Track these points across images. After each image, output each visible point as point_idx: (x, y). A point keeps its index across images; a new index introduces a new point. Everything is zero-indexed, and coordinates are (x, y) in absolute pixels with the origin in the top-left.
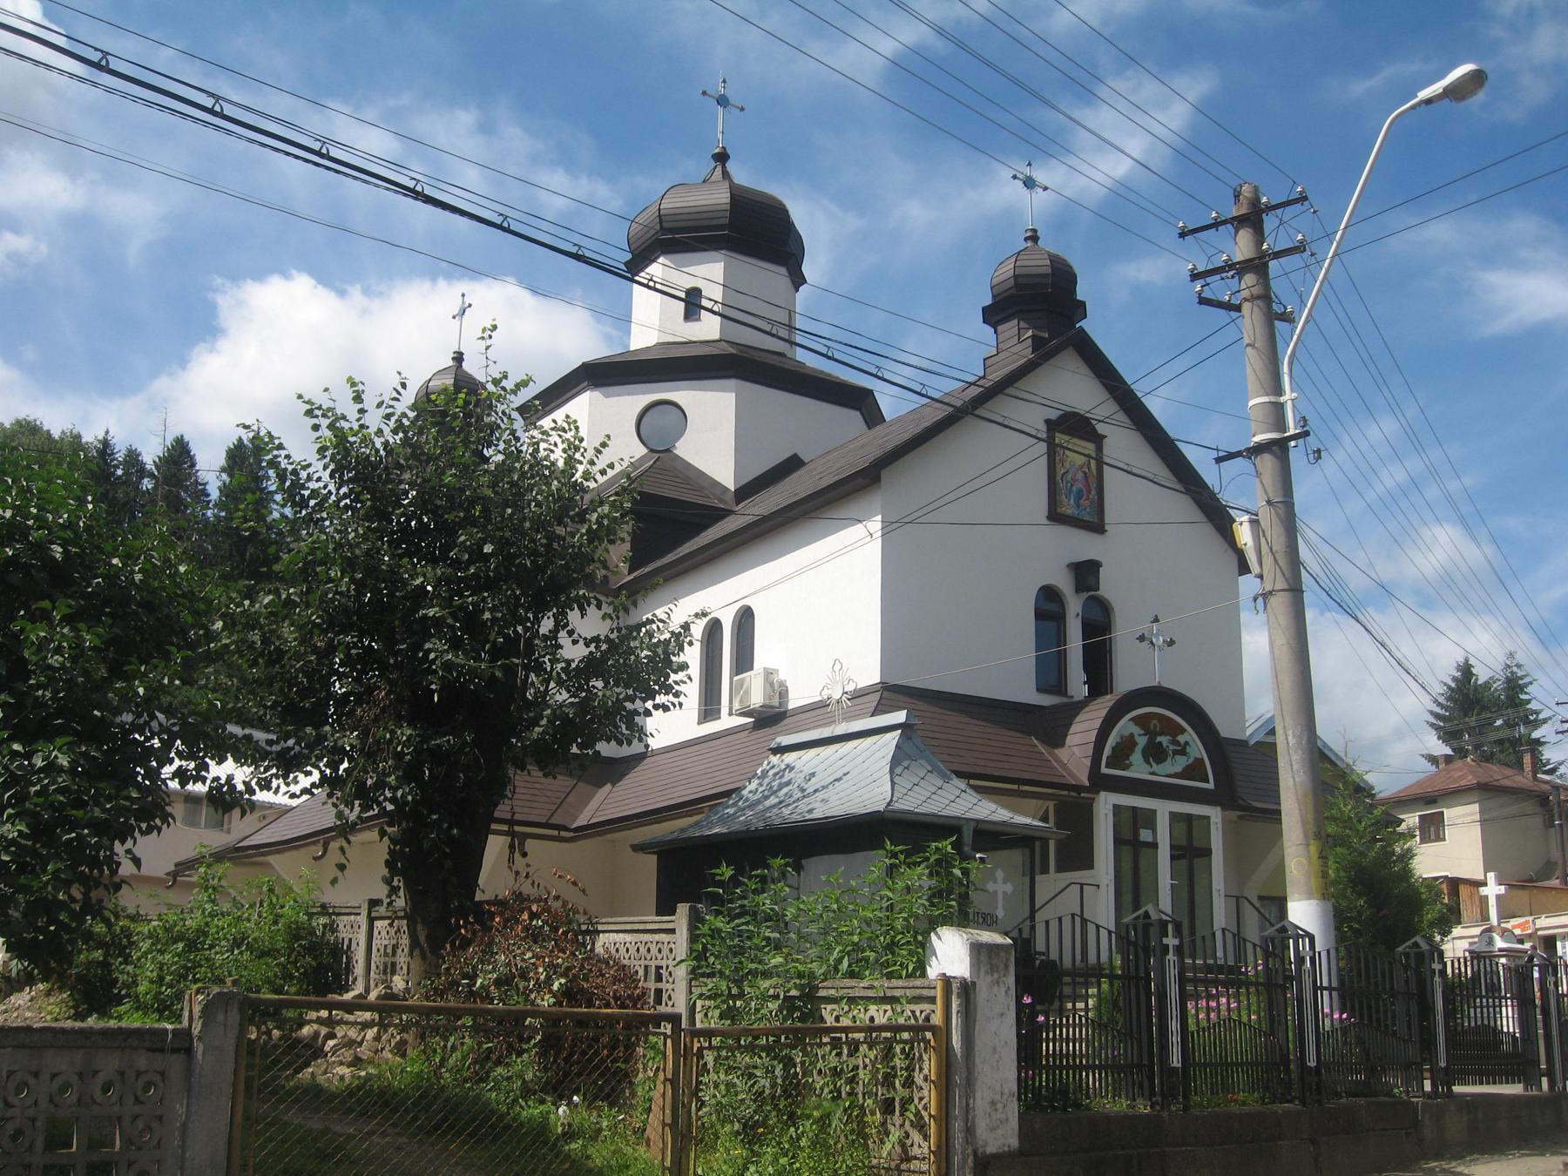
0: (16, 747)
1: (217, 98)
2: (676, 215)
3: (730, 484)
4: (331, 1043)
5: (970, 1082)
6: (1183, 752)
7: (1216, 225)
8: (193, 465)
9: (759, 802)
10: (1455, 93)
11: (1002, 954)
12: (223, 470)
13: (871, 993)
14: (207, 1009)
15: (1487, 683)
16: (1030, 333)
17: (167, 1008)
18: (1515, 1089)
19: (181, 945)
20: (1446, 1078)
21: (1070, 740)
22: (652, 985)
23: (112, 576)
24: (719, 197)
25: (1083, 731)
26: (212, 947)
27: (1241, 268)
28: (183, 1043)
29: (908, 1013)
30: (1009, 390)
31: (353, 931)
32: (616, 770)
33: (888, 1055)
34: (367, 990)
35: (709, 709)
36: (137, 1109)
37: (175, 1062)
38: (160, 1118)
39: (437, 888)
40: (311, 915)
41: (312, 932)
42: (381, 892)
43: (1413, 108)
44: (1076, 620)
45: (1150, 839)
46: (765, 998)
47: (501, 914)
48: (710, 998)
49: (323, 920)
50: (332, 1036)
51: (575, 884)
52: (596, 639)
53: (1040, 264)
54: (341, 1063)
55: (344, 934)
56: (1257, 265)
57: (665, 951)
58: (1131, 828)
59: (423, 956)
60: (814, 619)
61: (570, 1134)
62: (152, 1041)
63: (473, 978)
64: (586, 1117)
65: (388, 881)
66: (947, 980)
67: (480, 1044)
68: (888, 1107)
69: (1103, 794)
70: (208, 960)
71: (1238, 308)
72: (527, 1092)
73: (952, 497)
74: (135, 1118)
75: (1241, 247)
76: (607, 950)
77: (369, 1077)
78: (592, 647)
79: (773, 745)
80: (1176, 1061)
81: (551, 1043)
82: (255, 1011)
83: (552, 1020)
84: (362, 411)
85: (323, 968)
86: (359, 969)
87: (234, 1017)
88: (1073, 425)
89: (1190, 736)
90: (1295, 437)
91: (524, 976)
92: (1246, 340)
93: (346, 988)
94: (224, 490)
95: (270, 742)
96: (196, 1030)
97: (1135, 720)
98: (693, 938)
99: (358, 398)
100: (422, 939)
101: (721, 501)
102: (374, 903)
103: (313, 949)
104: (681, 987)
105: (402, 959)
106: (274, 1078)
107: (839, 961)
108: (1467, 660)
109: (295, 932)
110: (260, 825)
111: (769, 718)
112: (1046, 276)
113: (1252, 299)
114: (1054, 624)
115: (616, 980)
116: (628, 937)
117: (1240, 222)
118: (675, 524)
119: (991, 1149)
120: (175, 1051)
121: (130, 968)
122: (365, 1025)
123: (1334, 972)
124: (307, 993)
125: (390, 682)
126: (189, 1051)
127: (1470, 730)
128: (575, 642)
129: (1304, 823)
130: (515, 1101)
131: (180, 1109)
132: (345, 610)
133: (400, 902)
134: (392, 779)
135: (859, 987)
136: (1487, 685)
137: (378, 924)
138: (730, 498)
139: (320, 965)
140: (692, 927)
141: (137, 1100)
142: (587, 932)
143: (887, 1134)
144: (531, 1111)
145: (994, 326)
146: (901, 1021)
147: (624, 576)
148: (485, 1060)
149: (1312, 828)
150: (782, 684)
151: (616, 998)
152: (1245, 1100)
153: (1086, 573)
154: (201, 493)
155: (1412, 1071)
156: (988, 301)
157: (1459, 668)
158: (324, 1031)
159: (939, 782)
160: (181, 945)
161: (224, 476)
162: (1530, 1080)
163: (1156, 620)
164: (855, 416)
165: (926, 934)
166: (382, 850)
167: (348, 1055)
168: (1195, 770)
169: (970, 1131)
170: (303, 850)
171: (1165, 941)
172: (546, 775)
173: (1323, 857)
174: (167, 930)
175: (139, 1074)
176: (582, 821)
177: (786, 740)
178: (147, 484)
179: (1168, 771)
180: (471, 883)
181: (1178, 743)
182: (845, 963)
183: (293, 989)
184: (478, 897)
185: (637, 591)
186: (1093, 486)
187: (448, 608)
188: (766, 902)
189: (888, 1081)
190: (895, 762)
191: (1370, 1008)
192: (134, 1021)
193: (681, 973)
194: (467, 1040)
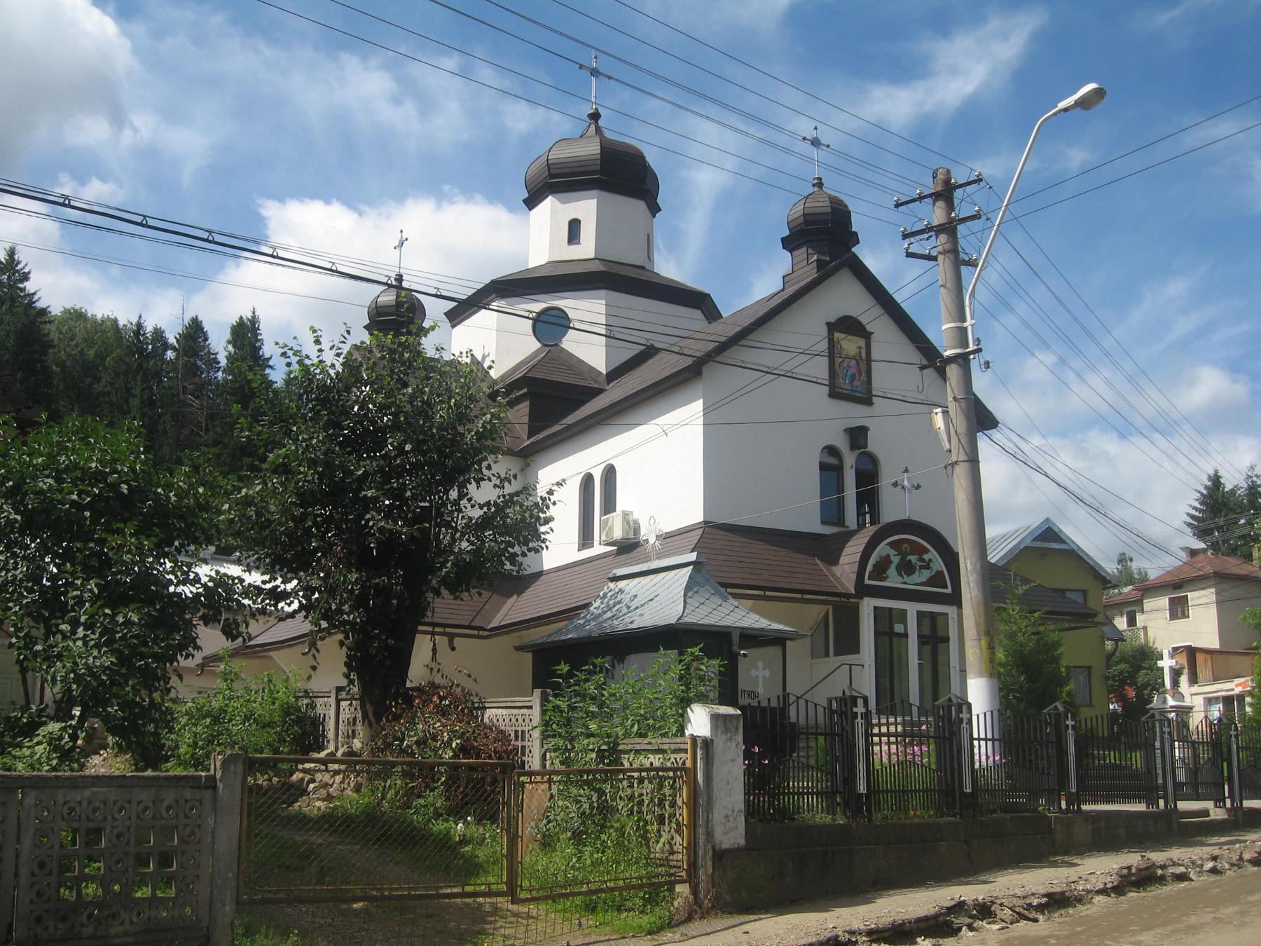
0: (107, 611)
1: (210, 232)
2: (561, 164)
3: (603, 369)
4: (312, 786)
5: (709, 805)
6: (928, 567)
7: (921, 198)
8: (206, 339)
9: (600, 615)
10: (1083, 103)
11: (734, 721)
12: (229, 342)
13: (649, 747)
14: (225, 764)
15: (1232, 490)
16: (815, 258)
17: (201, 764)
18: (1141, 807)
19: (208, 720)
20: (1074, 800)
21: (843, 560)
22: (519, 743)
23: (157, 498)
24: (592, 149)
25: (852, 552)
26: (230, 721)
27: (939, 229)
28: (211, 783)
29: (674, 759)
30: (743, 342)
31: (326, 708)
32: (521, 582)
33: (661, 787)
34: (337, 749)
35: (586, 538)
36: (186, 821)
37: (207, 794)
38: (199, 827)
39: (380, 679)
40: (297, 698)
41: (299, 710)
42: (344, 682)
43: (1055, 114)
44: (852, 473)
45: (902, 631)
46: (586, 751)
47: (420, 697)
48: (555, 751)
49: (306, 701)
50: (313, 781)
51: (469, 676)
52: (488, 504)
53: (822, 205)
54: (319, 799)
55: (320, 710)
56: (949, 229)
57: (527, 720)
58: (886, 623)
59: (370, 725)
60: (657, 474)
61: (464, 841)
62: (194, 783)
63: (402, 740)
64: (476, 831)
65: (347, 676)
66: (694, 739)
67: (407, 784)
68: (661, 819)
69: (866, 599)
70: (227, 730)
71: (935, 259)
72: (437, 815)
73: (744, 391)
74: (186, 826)
75: (937, 214)
76: (491, 720)
77: (336, 808)
78: (485, 509)
79: (611, 575)
80: (862, 789)
81: (453, 780)
82: (252, 766)
83: (454, 767)
84: (320, 350)
85: (307, 734)
86: (331, 735)
87: (240, 768)
88: (849, 325)
89: (933, 554)
90: (973, 352)
91: (434, 738)
92: (941, 282)
93: (321, 748)
94: (230, 358)
95: (264, 582)
96: (218, 777)
97: (891, 544)
98: (543, 712)
99: (317, 342)
100: (370, 714)
101: (596, 382)
102: (339, 689)
103: (299, 721)
104: (537, 743)
105: (359, 727)
106: (274, 812)
107: (632, 726)
108: (1216, 472)
109: (287, 710)
110: (261, 636)
111: (628, 547)
112: (827, 214)
113: (944, 252)
114: (834, 474)
115: (496, 740)
116: (504, 712)
117: (936, 196)
118: (556, 403)
119: (725, 846)
120: (206, 788)
121: (173, 736)
122: (336, 773)
123: (996, 722)
124: (295, 752)
125: (345, 541)
126: (215, 788)
127: (1219, 528)
128: (473, 506)
129: (977, 625)
130: (429, 820)
131: (211, 821)
132: (312, 493)
133: (355, 690)
134: (346, 607)
135: (642, 743)
136: (1233, 491)
137: (343, 703)
138: (602, 379)
139: (304, 733)
140: (542, 705)
141: (186, 816)
142: (479, 708)
143: (660, 836)
144: (439, 826)
145: (791, 251)
146: (669, 764)
147: (524, 441)
148: (411, 794)
149: (983, 628)
150: (636, 522)
151: (495, 752)
152: (918, 813)
153: (857, 436)
154: (212, 362)
155: (1053, 799)
156: (787, 233)
157: (1210, 478)
158: (308, 777)
159: (720, 601)
160: (208, 720)
161: (230, 348)
162: (1152, 801)
163: (906, 471)
164: (697, 314)
165: (685, 712)
166: (342, 654)
167: (323, 792)
168: (937, 580)
169: (709, 834)
170: (295, 648)
171: (855, 710)
172: (456, 598)
173: (991, 648)
174: (198, 709)
175: (186, 801)
176: (494, 624)
177: (620, 572)
178: (170, 355)
179: (916, 581)
180: (404, 676)
181: (924, 561)
182: (636, 727)
183: (286, 750)
184: (408, 685)
185: (530, 455)
186: (864, 370)
187: (384, 478)
188: (591, 688)
189: (661, 802)
190: (688, 588)
191: (1024, 751)
192: (179, 772)
193: (536, 734)
194: (399, 782)
